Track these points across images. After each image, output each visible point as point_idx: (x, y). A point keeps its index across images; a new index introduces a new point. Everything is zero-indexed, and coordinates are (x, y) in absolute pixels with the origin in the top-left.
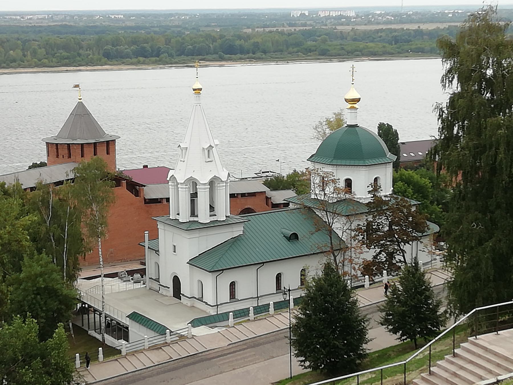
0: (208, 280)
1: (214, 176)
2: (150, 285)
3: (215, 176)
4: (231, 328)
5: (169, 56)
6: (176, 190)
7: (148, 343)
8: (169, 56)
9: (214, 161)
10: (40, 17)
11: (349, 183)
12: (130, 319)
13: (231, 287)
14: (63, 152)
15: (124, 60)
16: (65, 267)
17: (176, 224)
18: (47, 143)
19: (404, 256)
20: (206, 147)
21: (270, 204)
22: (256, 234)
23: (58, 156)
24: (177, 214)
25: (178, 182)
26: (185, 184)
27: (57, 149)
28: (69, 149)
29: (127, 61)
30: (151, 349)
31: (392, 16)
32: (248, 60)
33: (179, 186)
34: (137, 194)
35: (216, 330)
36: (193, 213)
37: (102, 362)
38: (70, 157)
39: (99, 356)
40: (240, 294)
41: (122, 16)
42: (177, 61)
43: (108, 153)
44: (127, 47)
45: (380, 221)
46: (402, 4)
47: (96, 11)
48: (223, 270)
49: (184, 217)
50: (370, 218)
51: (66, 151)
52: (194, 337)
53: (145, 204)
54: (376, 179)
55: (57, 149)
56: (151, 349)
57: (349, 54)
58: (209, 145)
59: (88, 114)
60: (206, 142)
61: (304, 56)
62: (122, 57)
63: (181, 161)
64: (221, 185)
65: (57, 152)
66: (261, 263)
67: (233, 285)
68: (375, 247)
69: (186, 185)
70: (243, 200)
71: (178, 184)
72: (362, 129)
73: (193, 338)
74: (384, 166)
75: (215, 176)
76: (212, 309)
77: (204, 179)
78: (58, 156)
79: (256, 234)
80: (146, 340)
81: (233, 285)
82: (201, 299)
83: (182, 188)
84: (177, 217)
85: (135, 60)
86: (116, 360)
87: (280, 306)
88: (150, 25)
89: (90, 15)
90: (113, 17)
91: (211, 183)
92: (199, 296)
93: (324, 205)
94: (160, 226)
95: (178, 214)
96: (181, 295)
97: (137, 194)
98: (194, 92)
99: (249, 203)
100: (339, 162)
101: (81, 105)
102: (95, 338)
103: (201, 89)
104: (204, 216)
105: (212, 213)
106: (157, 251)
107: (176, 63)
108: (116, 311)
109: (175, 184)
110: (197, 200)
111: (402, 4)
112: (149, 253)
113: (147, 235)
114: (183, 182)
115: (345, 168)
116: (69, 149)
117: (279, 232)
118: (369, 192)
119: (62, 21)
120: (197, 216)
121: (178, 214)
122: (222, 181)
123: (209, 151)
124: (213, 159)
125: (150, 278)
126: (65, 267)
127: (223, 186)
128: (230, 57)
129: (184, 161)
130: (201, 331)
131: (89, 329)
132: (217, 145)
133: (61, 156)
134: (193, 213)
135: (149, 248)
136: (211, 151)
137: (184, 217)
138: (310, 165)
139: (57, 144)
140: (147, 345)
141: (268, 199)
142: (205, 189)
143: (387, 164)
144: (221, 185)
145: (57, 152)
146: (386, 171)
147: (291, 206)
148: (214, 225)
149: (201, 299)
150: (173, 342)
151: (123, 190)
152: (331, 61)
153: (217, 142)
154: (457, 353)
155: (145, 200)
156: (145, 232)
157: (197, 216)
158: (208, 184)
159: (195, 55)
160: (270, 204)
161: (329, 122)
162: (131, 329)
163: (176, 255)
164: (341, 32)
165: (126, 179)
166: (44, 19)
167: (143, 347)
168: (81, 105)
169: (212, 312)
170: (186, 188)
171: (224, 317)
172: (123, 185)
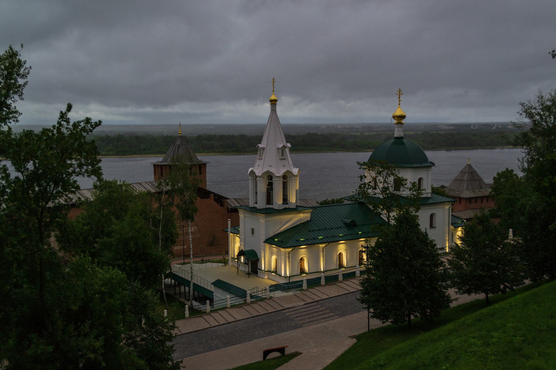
1: (286, 170)
3: (288, 171)
4: (305, 292)
6: (254, 182)
9: (287, 159)
22: (324, 214)
24: (256, 203)
27: (162, 169)
30: (232, 306)
33: (257, 179)
34: (222, 205)
36: (269, 199)
37: (188, 318)
46: (391, 122)
52: (272, 298)
54: (420, 180)
56: (232, 306)
58: (282, 145)
63: (259, 159)
69: (263, 178)
71: (256, 177)
73: (271, 299)
75: (288, 171)
77: (278, 172)
79: (324, 214)
83: (259, 180)
84: (256, 206)
86: (201, 316)
91: (284, 177)
95: (256, 203)
96: (258, 270)
104: (278, 201)
107: (248, 152)
109: (254, 178)
110: (273, 192)
111: (391, 122)
113: (229, 223)
114: (260, 175)
117: (340, 220)
120: (272, 204)
121: (256, 203)
123: (282, 151)
129: (262, 159)
130: (278, 294)
134: (269, 199)
137: (261, 204)
140: (229, 304)
142: (279, 181)
146: (428, 173)
150: (252, 302)
151: (211, 201)
152: (348, 151)
156: (229, 220)
157: (272, 204)
158: (282, 177)
163: (254, 236)
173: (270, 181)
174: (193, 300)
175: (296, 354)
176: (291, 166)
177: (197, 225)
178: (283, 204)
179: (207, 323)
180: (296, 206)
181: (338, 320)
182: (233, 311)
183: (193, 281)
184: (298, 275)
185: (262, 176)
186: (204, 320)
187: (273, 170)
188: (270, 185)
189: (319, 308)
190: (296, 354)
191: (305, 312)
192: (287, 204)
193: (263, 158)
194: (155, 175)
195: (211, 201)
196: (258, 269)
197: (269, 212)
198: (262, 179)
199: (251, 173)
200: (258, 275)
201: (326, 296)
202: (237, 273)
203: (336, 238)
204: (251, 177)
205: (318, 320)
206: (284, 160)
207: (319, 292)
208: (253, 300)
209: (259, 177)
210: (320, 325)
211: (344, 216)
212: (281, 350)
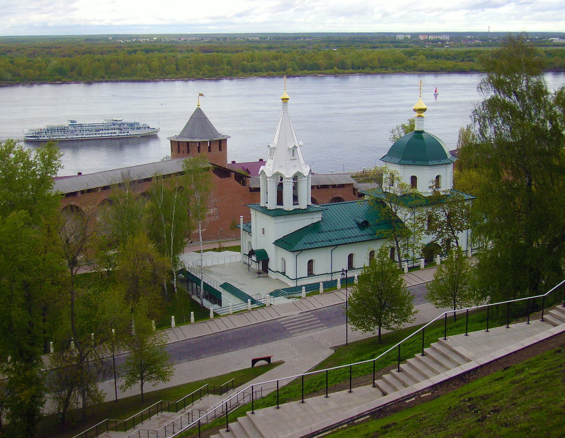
0: (289, 257)
1: (297, 171)
2: (244, 259)
5: (293, 70)
7: (232, 310)
8: (293, 70)
10: (193, 39)
11: (414, 179)
12: (222, 288)
13: (309, 264)
14: (183, 148)
15: (257, 74)
16: (172, 243)
17: (266, 211)
18: (171, 141)
19: (457, 242)
20: (291, 146)
21: (356, 194)
23: (179, 152)
25: (267, 176)
26: (272, 178)
27: (179, 146)
28: (188, 146)
29: (259, 74)
31: (480, 40)
32: (358, 74)
34: (244, 184)
35: (291, 300)
36: (280, 201)
37: (193, 324)
38: (188, 152)
39: (172, 323)
40: (317, 270)
41: (258, 38)
42: (300, 74)
43: (220, 150)
44: (259, 62)
45: (437, 212)
47: (238, 34)
48: (302, 250)
49: (272, 204)
50: (430, 210)
51: (186, 148)
53: (250, 192)
54: (438, 177)
55: (179, 146)
57: (442, 70)
58: (293, 146)
59: (205, 118)
60: (291, 143)
61: (404, 71)
62: (255, 71)
64: (303, 179)
65: (179, 148)
66: (335, 245)
67: (310, 263)
68: (432, 234)
70: (334, 190)
71: (267, 177)
72: (427, 133)
74: (445, 166)
76: (293, 282)
77: (288, 174)
78: (179, 152)
80: (231, 307)
81: (310, 263)
82: (284, 274)
85: (266, 74)
86: (205, 322)
87: (347, 282)
88: (281, 46)
89: (151, 36)
90: (251, 39)
91: (295, 178)
92: (282, 271)
93: (393, 198)
94: (253, 212)
95: (267, 203)
97: (244, 184)
98: (282, 101)
99: (339, 193)
100: (406, 162)
101: (199, 111)
102: (196, 302)
103: (288, 99)
104: (288, 205)
105: (295, 203)
106: (250, 233)
108: (212, 281)
109: (265, 177)
112: (244, 234)
115: (411, 167)
116: (188, 146)
118: (430, 187)
119: (210, 42)
121: (267, 203)
122: (304, 176)
124: (297, 157)
125: (244, 254)
126: (172, 243)
127: (305, 180)
128: (343, 72)
130: (281, 300)
131: (193, 294)
132: (301, 146)
133: (181, 152)
134: (280, 201)
135: (243, 229)
136: (295, 151)
137: (272, 204)
138: (382, 165)
139: (179, 142)
141: (354, 190)
143: (448, 164)
144: (303, 179)
145: (179, 148)
146: (447, 170)
147: (366, 198)
148: (297, 212)
149: (284, 274)
151: (231, 180)
153: (301, 143)
154: (544, 318)
155: (250, 189)
159: (315, 69)
160: (356, 194)
161: (404, 127)
162: (224, 297)
164: (437, 53)
165: (234, 172)
166: (196, 40)
167: (228, 313)
168: (199, 111)
169: (292, 284)
170: (273, 181)
171: (298, 289)
172: (232, 176)
173: (281, 182)
174: (203, 298)
175: (281, 363)
176: (302, 166)
177: (216, 207)
178: (294, 204)
179: (209, 329)
180: (307, 205)
181: (325, 330)
182: (235, 318)
183: (204, 280)
184: (306, 277)
185: (272, 177)
186: (208, 327)
187: (282, 172)
188: (280, 186)
189: (312, 318)
190: (281, 363)
191: (299, 321)
192: (298, 204)
193: (274, 157)
194: (172, 151)
195: (231, 180)
196: (269, 269)
197: (278, 213)
198: (272, 180)
199: (262, 173)
200: (268, 274)
201: (321, 305)
202: (248, 272)
203: (345, 240)
204: (262, 177)
205: (316, 328)
206: (294, 161)
207: (316, 301)
208: (255, 306)
209: (270, 177)
210: (307, 335)
211: (359, 215)
212: (268, 359)
